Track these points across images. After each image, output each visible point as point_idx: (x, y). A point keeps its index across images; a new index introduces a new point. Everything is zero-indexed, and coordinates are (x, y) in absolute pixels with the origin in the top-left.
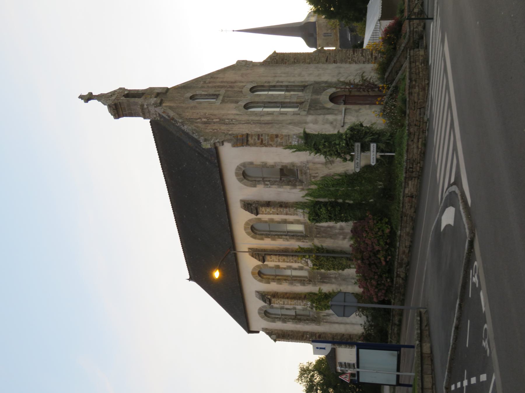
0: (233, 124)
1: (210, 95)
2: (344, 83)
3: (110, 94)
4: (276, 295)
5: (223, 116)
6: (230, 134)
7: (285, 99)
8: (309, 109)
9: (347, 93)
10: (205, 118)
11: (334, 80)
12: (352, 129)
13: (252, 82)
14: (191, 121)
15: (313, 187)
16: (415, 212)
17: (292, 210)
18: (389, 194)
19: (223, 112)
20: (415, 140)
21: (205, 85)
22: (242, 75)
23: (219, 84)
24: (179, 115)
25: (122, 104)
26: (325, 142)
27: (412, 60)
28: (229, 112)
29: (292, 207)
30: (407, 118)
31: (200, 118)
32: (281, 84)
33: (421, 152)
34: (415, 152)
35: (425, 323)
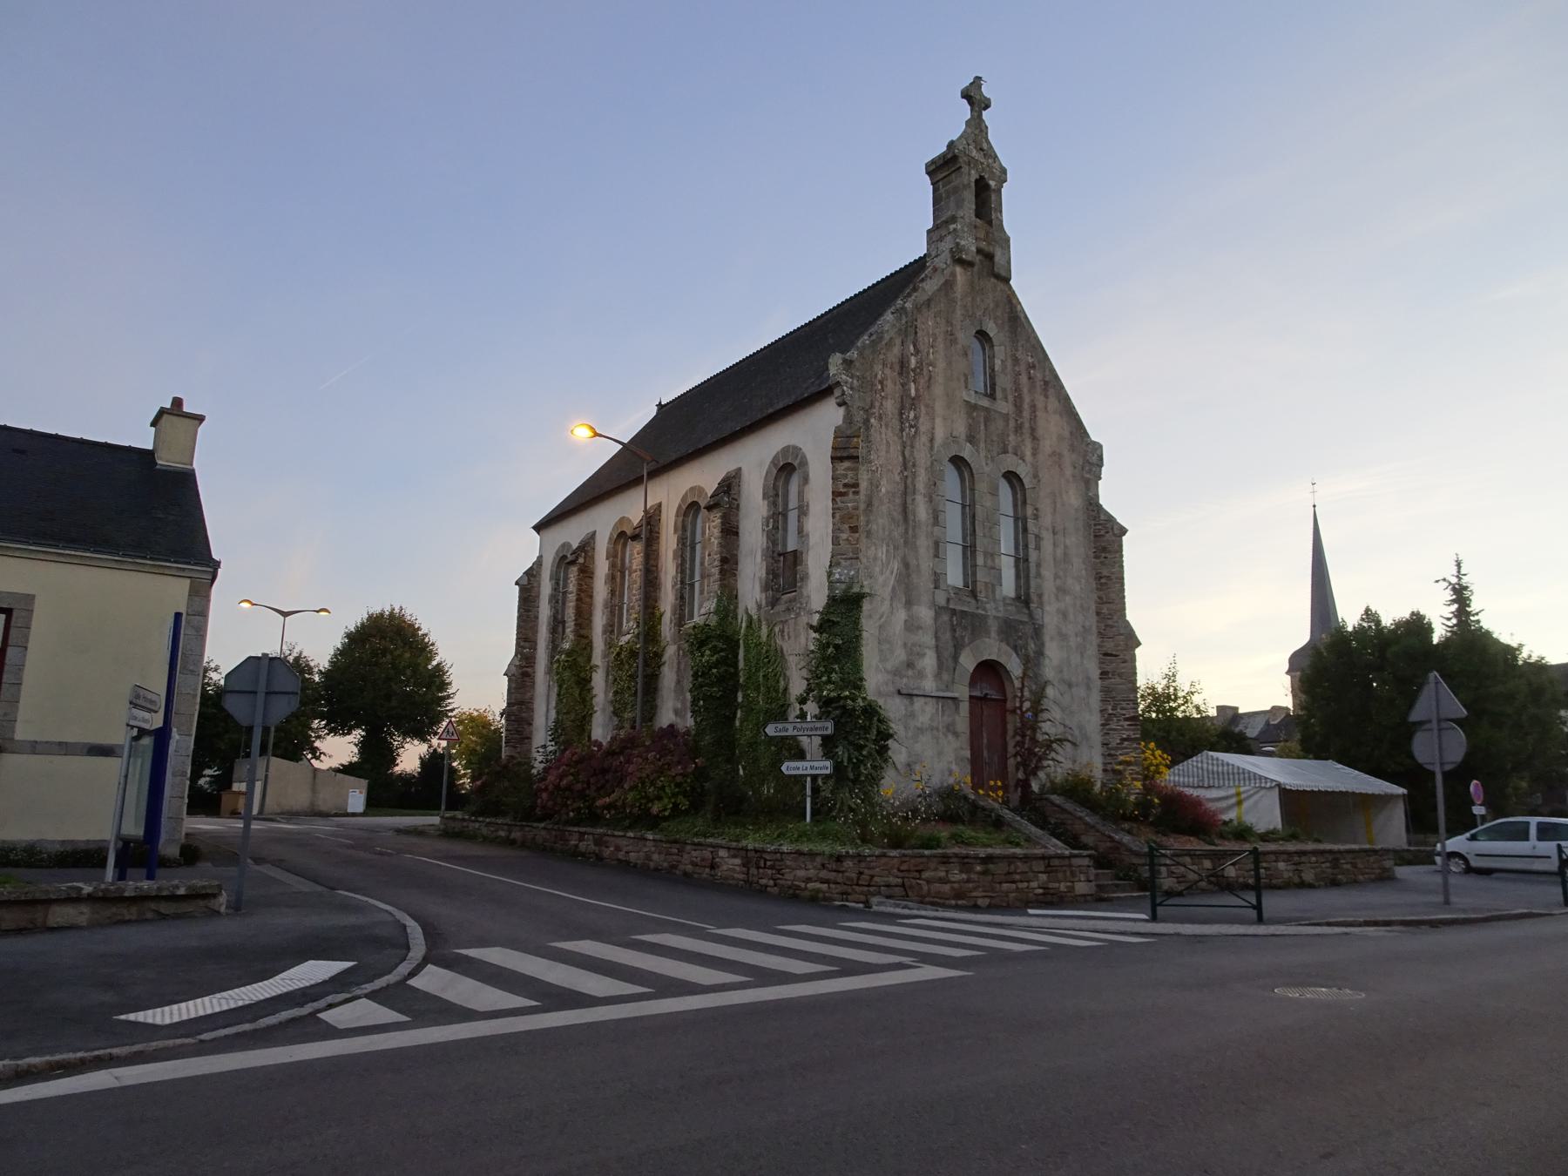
0: (902, 430)
1: (992, 378)
2: (1038, 697)
3: (985, 146)
4: (587, 573)
5: (927, 406)
6: (867, 421)
7: (986, 554)
8: (954, 612)
9: (1009, 705)
10: (920, 364)
11: (1049, 672)
12: (871, 711)
13: (1036, 476)
14: (909, 331)
15: (764, 631)
16: (685, 874)
17: (715, 587)
18: (733, 808)
19: (939, 407)
20: (824, 874)
21: (1023, 368)
22: (1056, 455)
23: (1027, 400)
24: (928, 303)
25: (966, 182)
26: (837, 647)
27: (1056, 862)
28: (938, 421)
29: (722, 586)
30: (878, 852)
31: (917, 351)
32: (1032, 546)
33: (798, 888)
34: (797, 874)
35: (164, 908)
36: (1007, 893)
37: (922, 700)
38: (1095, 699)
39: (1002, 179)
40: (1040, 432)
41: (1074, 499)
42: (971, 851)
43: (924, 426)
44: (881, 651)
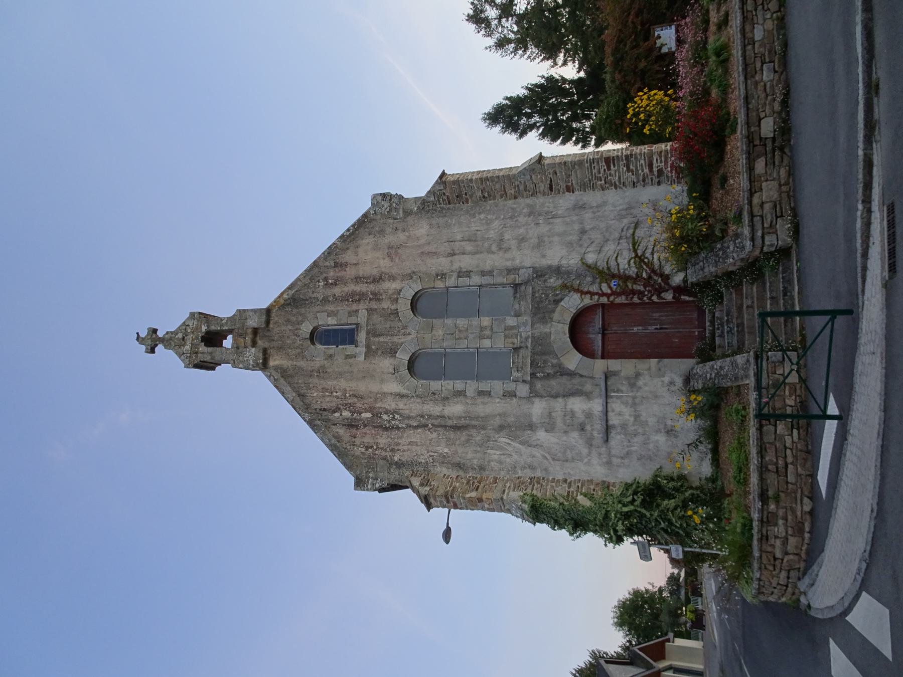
0: (398, 428)
5: (376, 400)
8: (533, 375)
10: (348, 406)
11: (572, 261)
13: (410, 276)
19: (375, 387)
21: (329, 292)
23: (352, 287)
36: (798, 475)
37: (610, 414)
38: (592, 197)
39: (205, 317)
40: (375, 272)
41: (422, 229)
42: (756, 516)
43: (390, 404)
44: (573, 459)
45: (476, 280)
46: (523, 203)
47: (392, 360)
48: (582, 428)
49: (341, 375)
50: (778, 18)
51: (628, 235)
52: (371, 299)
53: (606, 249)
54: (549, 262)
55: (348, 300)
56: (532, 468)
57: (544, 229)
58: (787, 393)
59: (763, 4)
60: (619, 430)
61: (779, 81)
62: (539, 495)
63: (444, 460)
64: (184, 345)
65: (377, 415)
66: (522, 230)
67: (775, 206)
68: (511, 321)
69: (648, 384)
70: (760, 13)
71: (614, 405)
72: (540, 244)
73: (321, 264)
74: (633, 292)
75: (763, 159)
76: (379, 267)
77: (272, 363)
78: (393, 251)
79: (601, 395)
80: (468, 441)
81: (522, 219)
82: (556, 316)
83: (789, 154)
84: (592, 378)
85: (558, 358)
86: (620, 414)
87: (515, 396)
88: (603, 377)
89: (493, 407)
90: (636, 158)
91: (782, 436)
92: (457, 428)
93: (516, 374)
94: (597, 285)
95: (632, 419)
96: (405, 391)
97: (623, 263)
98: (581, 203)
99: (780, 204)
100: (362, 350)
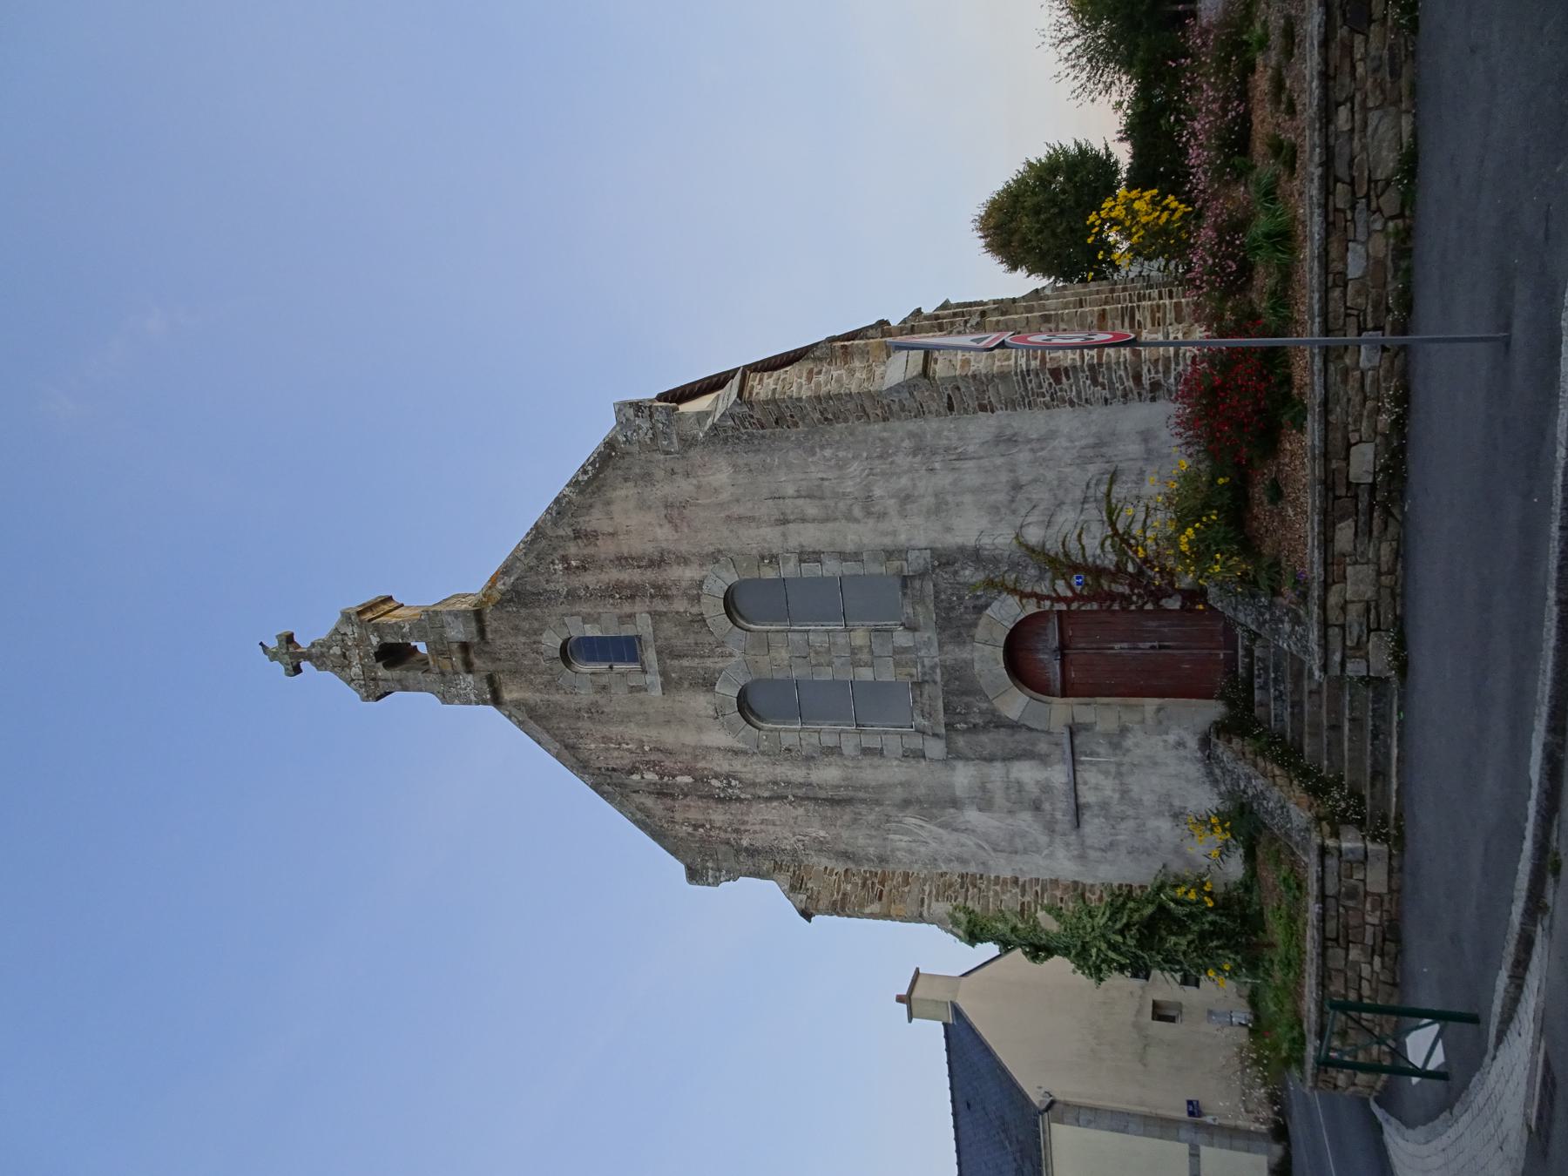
0: (739, 799)
10: (652, 765)
11: (1001, 539)
19: (689, 738)
23: (615, 575)
37: (1080, 787)
38: (1030, 422)
43: (722, 765)
44: (1025, 851)
45: (832, 568)
46: (901, 428)
47: (709, 697)
48: (1037, 807)
49: (626, 718)
50: (1397, 233)
51: (1099, 495)
52: (652, 596)
53: (1060, 518)
54: (960, 540)
55: (612, 596)
56: (962, 861)
57: (944, 480)
58: (1368, 907)
59: (1367, 196)
60: (1096, 810)
61: (1390, 371)
62: (978, 909)
63: (821, 846)
64: (349, 666)
65: (700, 779)
66: (904, 481)
67: (1368, 610)
68: (902, 638)
69: (1141, 744)
70: (1361, 217)
71: (1086, 775)
72: (939, 508)
73: (549, 532)
74: (1112, 596)
75: (1350, 522)
76: (655, 540)
77: (506, 696)
78: (675, 512)
79: (1063, 761)
80: (855, 821)
81: (903, 460)
82: (980, 632)
83: (1399, 517)
84: (1048, 733)
85: (989, 701)
86: (1096, 788)
87: (924, 757)
88: (1067, 734)
89: (892, 772)
90: (1109, 368)
91: (1357, 963)
92: (833, 802)
93: (921, 721)
94: (1047, 583)
95: (1117, 796)
96: (741, 745)
97: (1092, 544)
98: (1008, 432)
99: (1377, 608)
100: (654, 679)
